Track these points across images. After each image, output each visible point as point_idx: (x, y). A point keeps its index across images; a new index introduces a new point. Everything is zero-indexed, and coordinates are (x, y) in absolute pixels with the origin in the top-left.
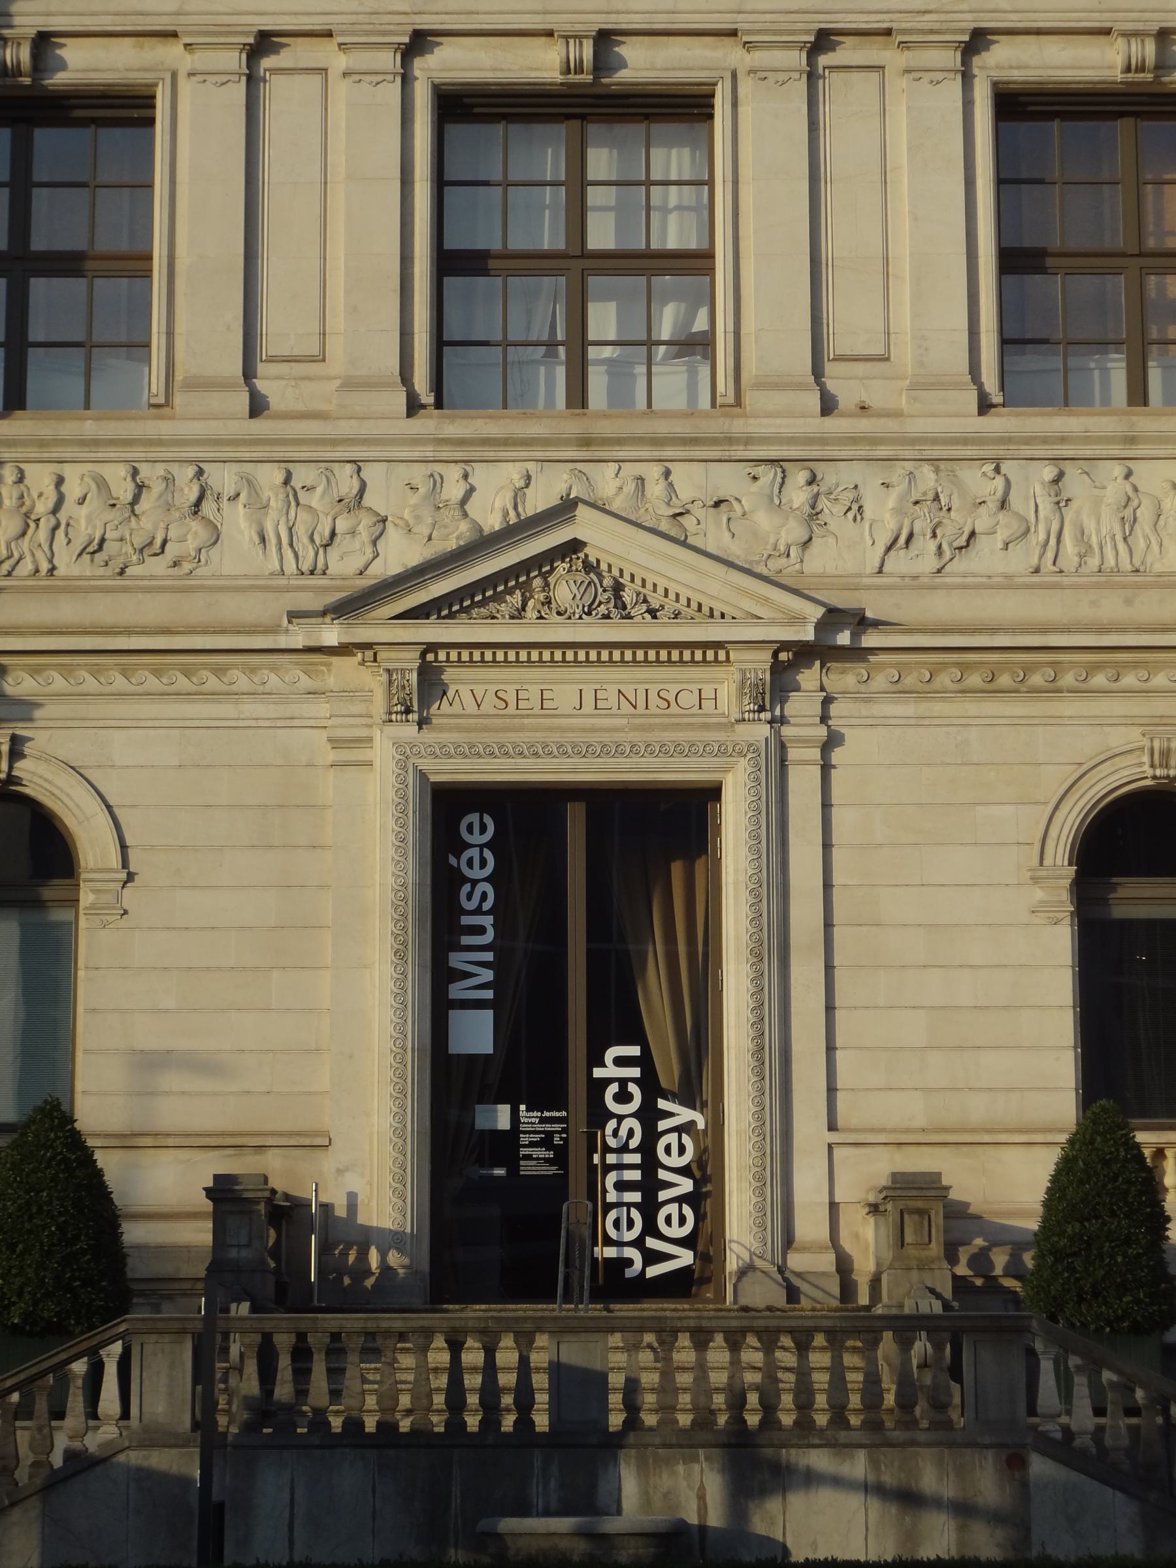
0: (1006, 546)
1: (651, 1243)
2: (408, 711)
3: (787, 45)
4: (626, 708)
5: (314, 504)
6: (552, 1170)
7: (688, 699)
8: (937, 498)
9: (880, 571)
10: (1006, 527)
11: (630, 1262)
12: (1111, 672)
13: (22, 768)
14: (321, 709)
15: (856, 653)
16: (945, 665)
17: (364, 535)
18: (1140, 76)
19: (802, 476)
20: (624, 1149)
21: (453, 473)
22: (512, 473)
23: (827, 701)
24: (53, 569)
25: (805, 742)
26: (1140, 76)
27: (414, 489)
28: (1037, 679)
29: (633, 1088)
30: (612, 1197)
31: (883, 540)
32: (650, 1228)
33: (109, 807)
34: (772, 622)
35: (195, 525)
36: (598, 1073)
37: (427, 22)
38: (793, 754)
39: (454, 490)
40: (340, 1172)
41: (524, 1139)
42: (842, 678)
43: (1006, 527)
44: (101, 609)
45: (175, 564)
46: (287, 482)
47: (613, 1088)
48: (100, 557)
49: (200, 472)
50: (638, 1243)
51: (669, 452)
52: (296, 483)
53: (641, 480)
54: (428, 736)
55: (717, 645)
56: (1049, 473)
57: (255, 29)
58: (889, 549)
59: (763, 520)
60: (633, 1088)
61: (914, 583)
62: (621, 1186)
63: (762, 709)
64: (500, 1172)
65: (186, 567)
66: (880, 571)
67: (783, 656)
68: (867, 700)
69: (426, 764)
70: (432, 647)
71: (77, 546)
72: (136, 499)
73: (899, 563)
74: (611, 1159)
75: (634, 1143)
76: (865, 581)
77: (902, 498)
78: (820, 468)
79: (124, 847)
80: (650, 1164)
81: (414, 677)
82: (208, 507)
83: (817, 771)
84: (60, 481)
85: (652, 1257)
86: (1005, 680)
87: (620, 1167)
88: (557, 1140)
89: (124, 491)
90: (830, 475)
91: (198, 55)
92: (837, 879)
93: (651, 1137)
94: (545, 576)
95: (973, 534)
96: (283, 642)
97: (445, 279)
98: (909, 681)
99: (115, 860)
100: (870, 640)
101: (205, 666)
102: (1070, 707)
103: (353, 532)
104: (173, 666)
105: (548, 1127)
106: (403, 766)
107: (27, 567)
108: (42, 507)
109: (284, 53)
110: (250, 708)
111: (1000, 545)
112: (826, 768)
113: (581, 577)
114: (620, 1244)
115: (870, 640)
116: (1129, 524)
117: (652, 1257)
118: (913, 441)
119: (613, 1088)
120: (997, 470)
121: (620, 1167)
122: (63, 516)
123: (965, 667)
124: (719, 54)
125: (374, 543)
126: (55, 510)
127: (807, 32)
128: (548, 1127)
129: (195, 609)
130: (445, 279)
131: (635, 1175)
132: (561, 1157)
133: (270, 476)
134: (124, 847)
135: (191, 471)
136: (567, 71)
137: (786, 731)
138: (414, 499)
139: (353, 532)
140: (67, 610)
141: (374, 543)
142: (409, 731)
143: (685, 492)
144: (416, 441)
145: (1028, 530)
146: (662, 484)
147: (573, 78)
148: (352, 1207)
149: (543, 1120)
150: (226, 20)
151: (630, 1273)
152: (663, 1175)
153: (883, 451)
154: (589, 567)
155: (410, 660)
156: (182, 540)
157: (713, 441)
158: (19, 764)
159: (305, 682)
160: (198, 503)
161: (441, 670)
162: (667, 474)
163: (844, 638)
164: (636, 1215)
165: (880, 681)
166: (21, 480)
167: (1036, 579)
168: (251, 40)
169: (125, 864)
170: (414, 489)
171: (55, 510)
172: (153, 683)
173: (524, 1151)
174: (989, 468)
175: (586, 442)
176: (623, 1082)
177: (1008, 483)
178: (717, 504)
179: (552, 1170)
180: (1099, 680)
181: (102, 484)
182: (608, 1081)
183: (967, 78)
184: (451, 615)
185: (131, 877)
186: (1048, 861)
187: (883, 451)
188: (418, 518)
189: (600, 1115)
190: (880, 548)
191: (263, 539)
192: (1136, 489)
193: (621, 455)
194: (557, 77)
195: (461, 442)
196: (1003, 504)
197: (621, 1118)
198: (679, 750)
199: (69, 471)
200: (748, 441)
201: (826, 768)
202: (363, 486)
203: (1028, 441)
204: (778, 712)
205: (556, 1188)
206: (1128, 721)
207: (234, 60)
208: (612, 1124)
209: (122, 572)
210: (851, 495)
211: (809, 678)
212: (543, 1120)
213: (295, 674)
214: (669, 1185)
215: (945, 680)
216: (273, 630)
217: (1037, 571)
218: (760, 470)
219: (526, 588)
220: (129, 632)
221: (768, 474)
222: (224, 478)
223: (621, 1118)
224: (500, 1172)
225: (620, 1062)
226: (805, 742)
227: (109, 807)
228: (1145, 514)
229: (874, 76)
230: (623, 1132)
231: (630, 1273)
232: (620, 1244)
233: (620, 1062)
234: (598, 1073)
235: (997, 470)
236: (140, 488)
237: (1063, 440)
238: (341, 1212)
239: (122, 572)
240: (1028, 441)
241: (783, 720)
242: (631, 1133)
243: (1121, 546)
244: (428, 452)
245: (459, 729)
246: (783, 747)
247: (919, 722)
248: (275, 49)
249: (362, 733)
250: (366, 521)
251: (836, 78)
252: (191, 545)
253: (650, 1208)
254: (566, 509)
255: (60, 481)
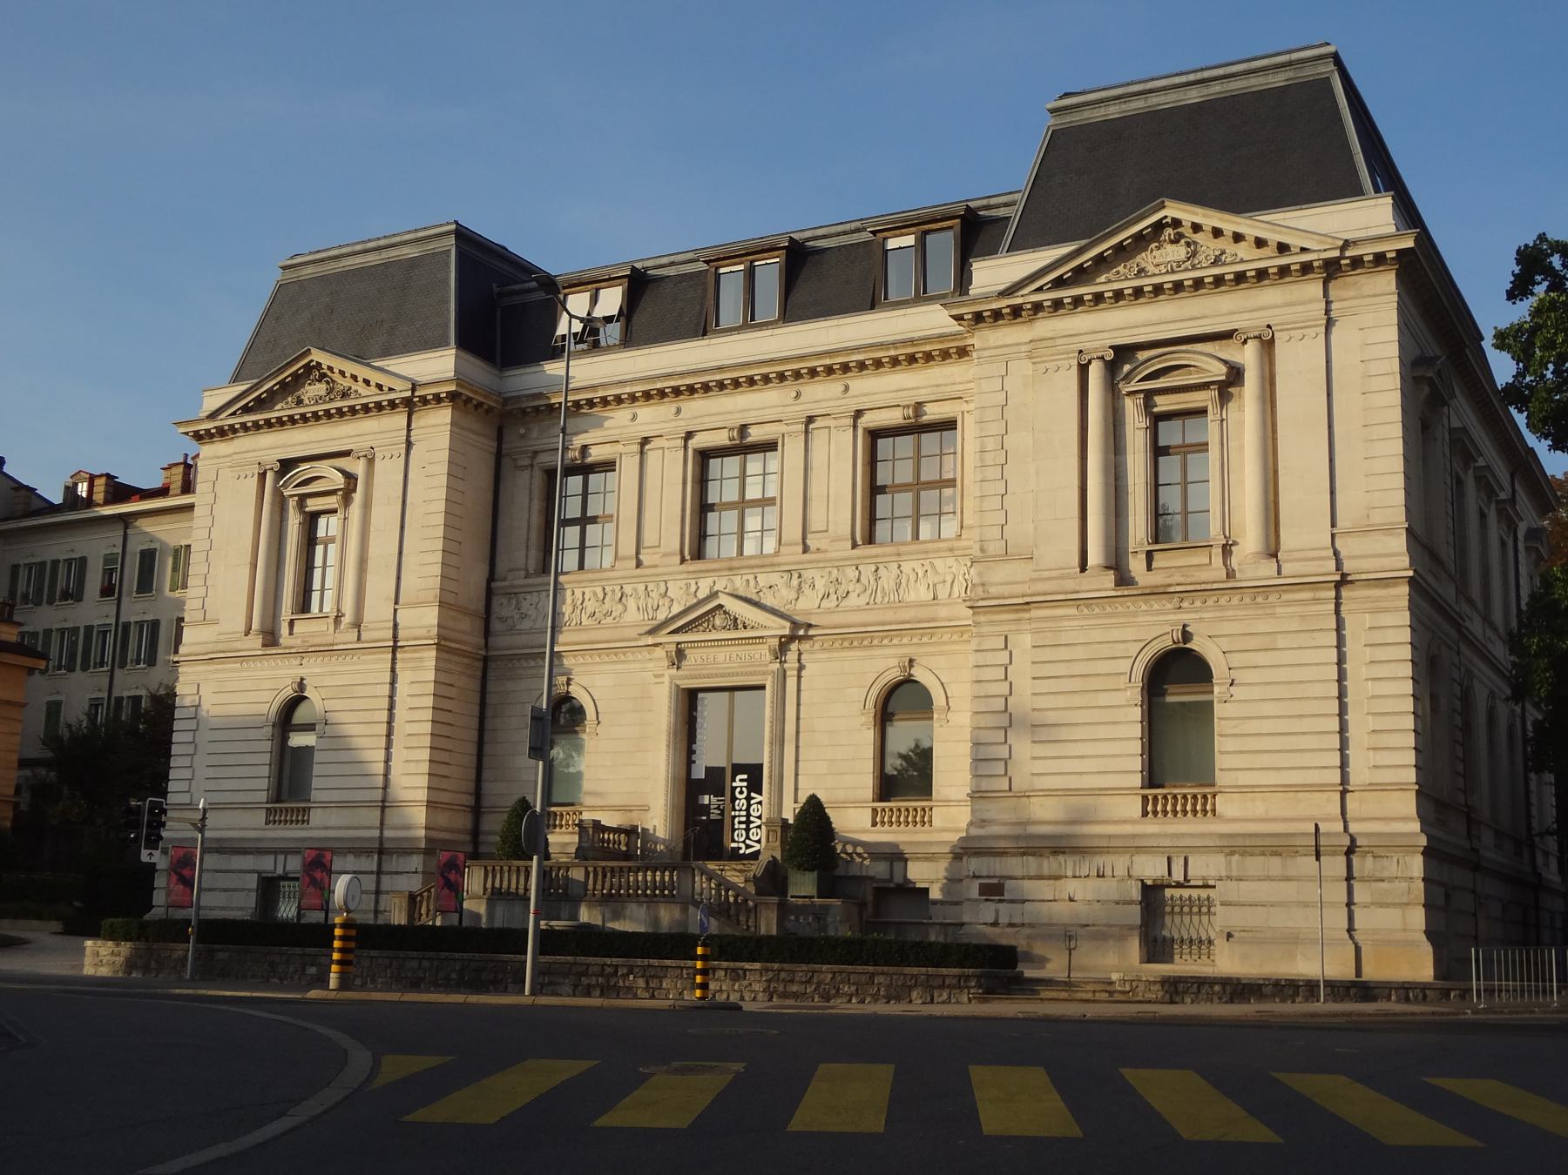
0: (859, 595)
1: (748, 842)
2: (674, 664)
3: (798, 423)
4: (739, 660)
5: (654, 596)
6: (720, 817)
7: (757, 656)
8: (837, 580)
9: (819, 607)
10: (859, 588)
11: (741, 848)
12: (889, 639)
13: (571, 688)
14: (651, 665)
15: (807, 637)
16: (837, 639)
17: (667, 606)
18: (910, 421)
19: (797, 575)
20: (741, 810)
21: (693, 582)
22: (709, 581)
23: (800, 654)
24: (581, 624)
25: (792, 669)
26: (910, 421)
27: (681, 588)
28: (865, 643)
29: (744, 789)
30: (736, 827)
31: (820, 596)
32: (748, 837)
33: (594, 700)
34: (776, 629)
35: (620, 606)
36: (734, 784)
37: (690, 429)
38: (788, 673)
39: (693, 588)
40: (652, 818)
41: (712, 807)
42: (805, 646)
43: (859, 588)
44: (593, 635)
45: (614, 619)
46: (646, 589)
47: (738, 789)
48: (594, 618)
49: (622, 588)
50: (744, 842)
51: (756, 571)
52: (649, 589)
53: (748, 581)
54: (680, 672)
55: (762, 637)
56: (873, 568)
57: (805, 416)
58: (822, 600)
59: (784, 592)
60: (744, 789)
61: (830, 611)
62: (740, 823)
63: (777, 658)
64: (704, 818)
65: (617, 619)
66: (819, 607)
67: (783, 640)
68: (812, 653)
69: (678, 682)
70: (679, 643)
71: (588, 615)
72: (604, 599)
73: (825, 604)
74: (737, 813)
75: (744, 808)
76: (814, 611)
77: (826, 581)
78: (802, 572)
79: (597, 713)
80: (748, 815)
81: (674, 653)
82: (624, 599)
83: (796, 678)
84: (584, 593)
85: (748, 847)
86: (855, 643)
87: (739, 816)
88: (721, 807)
89: (601, 595)
90: (805, 574)
91: (627, 447)
92: (801, 716)
93: (749, 806)
94: (714, 617)
95: (848, 592)
96: (640, 643)
97: (1160, 458)
98: (826, 645)
99: (595, 718)
100: (811, 632)
101: (621, 652)
102: (879, 652)
103: (664, 605)
104: (612, 653)
105: (719, 803)
106: (671, 683)
107: (574, 623)
108: (579, 603)
109: (652, 443)
110: (633, 666)
111: (856, 595)
112: (799, 677)
113: (723, 616)
114: (738, 842)
115: (811, 632)
116: (898, 585)
117: (748, 847)
118: (830, 561)
119: (738, 789)
120: (857, 569)
121: (739, 816)
122: (584, 605)
123: (843, 640)
124: (779, 428)
125: (670, 608)
126: (582, 604)
127: (851, 412)
128: (719, 803)
129: (617, 634)
130: (1160, 458)
131: (744, 819)
132: (722, 814)
133: (641, 587)
134: (597, 713)
135: (619, 587)
136: (905, 419)
137: (786, 665)
138: (682, 592)
139: (664, 605)
140: (583, 636)
141: (670, 608)
142: (673, 671)
143: (761, 583)
144: (681, 573)
145: (866, 589)
146: (754, 581)
147: (734, 442)
148: (655, 830)
149: (718, 801)
150: (633, 435)
151: (741, 852)
152: (752, 819)
153: (821, 565)
154: (725, 613)
155: (673, 648)
156: (616, 611)
157: (767, 566)
158: (570, 687)
159: (648, 656)
160: (621, 599)
161: (684, 650)
162: (756, 577)
163: (801, 632)
164: (744, 832)
165: (817, 646)
166: (573, 594)
167: (868, 607)
168: (640, 441)
169: (598, 719)
170: (681, 588)
171: (582, 604)
172: (606, 659)
173: (712, 811)
174: (854, 568)
175: (730, 569)
176: (741, 787)
177: (860, 572)
178: (770, 587)
179: (720, 817)
180: (886, 642)
181: (595, 593)
182: (736, 787)
183: (855, 427)
184: (686, 632)
185: (599, 723)
186: (1133, 680)
187: (821, 565)
188: (682, 599)
189: (734, 799)
190: (819, 599)
191: (639, 609)
192: (901, 572)
193: (742, 572)
194: (727, 442)
195: (694, 572)
196: (858, 581)
197: (740, 800)
198: (751, 674)
199: (586, 590)
200: (779, 565)
201: (799, 677)
202: (667, 588)
203: (865, 558)
204: (783, 659)
205: (720, 822)
206: (895, 656)
207: (636, 448)
208: (737, 802)
209: (599, 623)
210: (811, 581)
211: (794, 646)
212: (718, 801)
213: (645, 654)
214: (753, 822)
215: (837, 645)
216: (635, 640)
217: (868, 604)
218: (783, 574)
219: (708, 620)
220: (598, 642)
221: (786, 575)
222: (628, 589)
223: (740, 800)
224: (704, 818)
225: (741, 780)
226: (792, 669)
227: (594, 700)
228: (904, 581)
229: (827, 430)
230: (741, 805)
231: (741, 852)
232: (738, 842)
233: (741, 780)
234: (734, 784)
235: (857, 569)
236: (605, 594)
237: (877, 556)
238: (651, 832)
239: (599, 623)
240: (865, 558)
241: (785, 662)
242: (743, 805)
243: (896, 593)
244: (685, 576)
245: (689, 670)
246: (785, 671)
247: (829, 660)
248: (649, 442)
249: (661, 672)
250: (667, 600)
251: (649, 453)
252: (619, 612)
253: (748, 830)
254: (713, 595)
255: (584, 593)
